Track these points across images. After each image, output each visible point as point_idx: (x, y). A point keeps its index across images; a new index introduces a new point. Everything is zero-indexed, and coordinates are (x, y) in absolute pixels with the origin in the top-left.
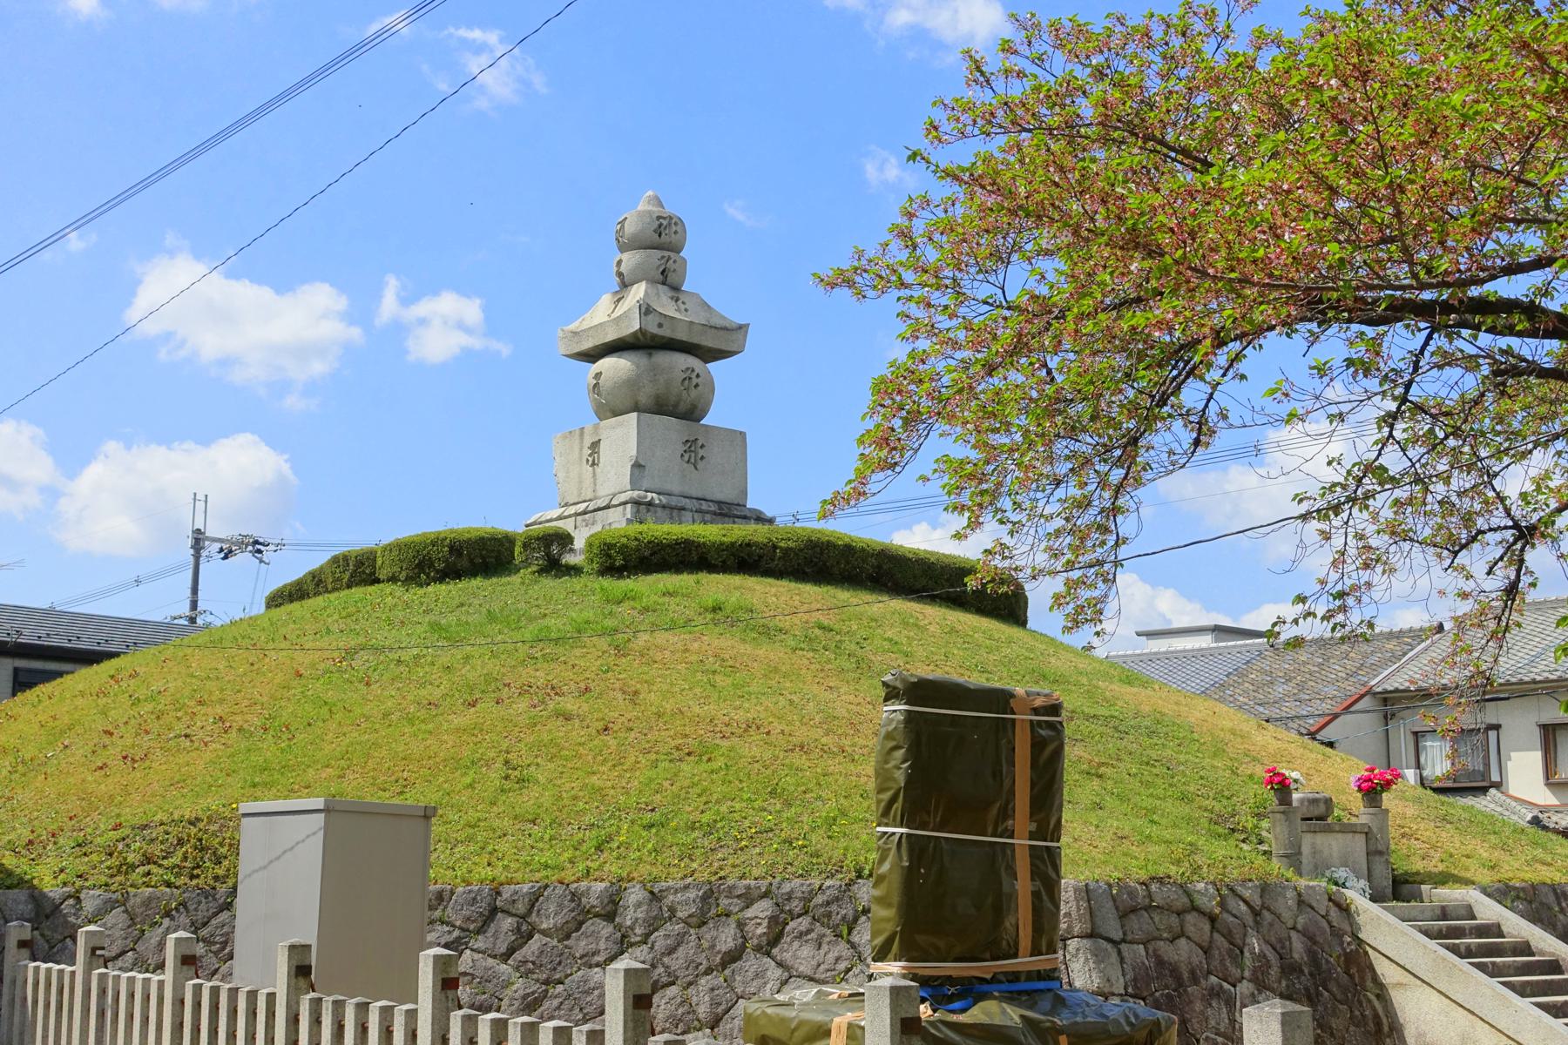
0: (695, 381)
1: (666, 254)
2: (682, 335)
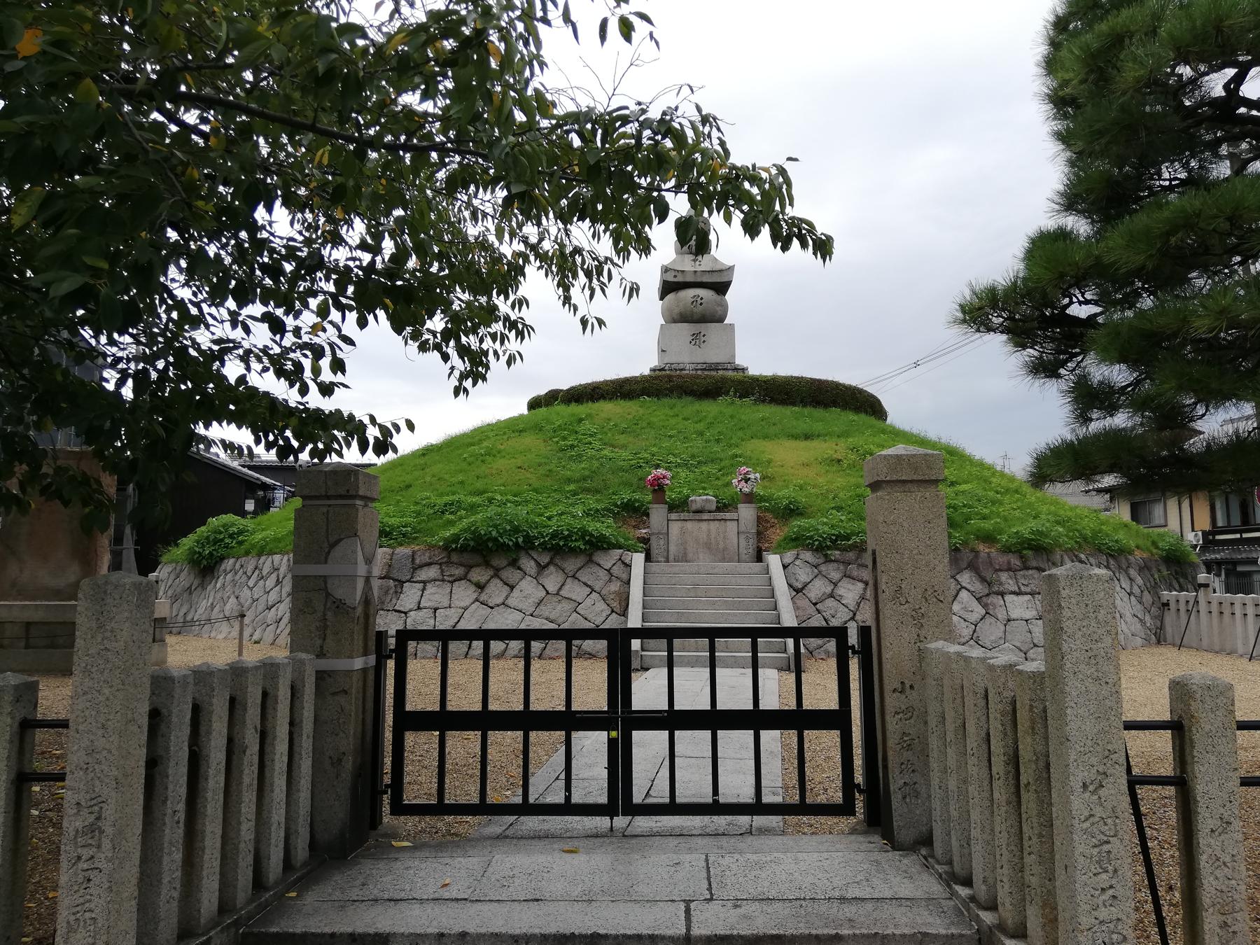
2: (689, 279)
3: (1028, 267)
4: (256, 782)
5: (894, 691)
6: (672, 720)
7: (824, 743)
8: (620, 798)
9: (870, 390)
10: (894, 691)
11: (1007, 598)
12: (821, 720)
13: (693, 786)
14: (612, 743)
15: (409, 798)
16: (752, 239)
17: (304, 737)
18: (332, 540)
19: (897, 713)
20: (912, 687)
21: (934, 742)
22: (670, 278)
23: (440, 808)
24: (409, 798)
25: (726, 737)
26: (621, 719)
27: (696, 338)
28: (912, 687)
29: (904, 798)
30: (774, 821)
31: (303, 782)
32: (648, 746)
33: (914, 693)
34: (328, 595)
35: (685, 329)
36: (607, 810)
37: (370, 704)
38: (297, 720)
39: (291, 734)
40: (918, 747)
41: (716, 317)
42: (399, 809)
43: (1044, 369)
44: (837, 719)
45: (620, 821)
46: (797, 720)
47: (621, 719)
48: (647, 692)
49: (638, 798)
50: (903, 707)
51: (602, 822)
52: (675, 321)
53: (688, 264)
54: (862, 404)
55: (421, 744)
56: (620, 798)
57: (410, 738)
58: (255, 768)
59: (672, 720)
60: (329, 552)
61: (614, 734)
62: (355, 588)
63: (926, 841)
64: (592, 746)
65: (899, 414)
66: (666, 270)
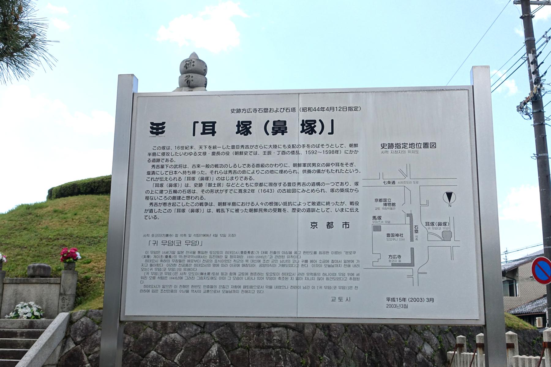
1: (188, 74)
16: (194, 54)
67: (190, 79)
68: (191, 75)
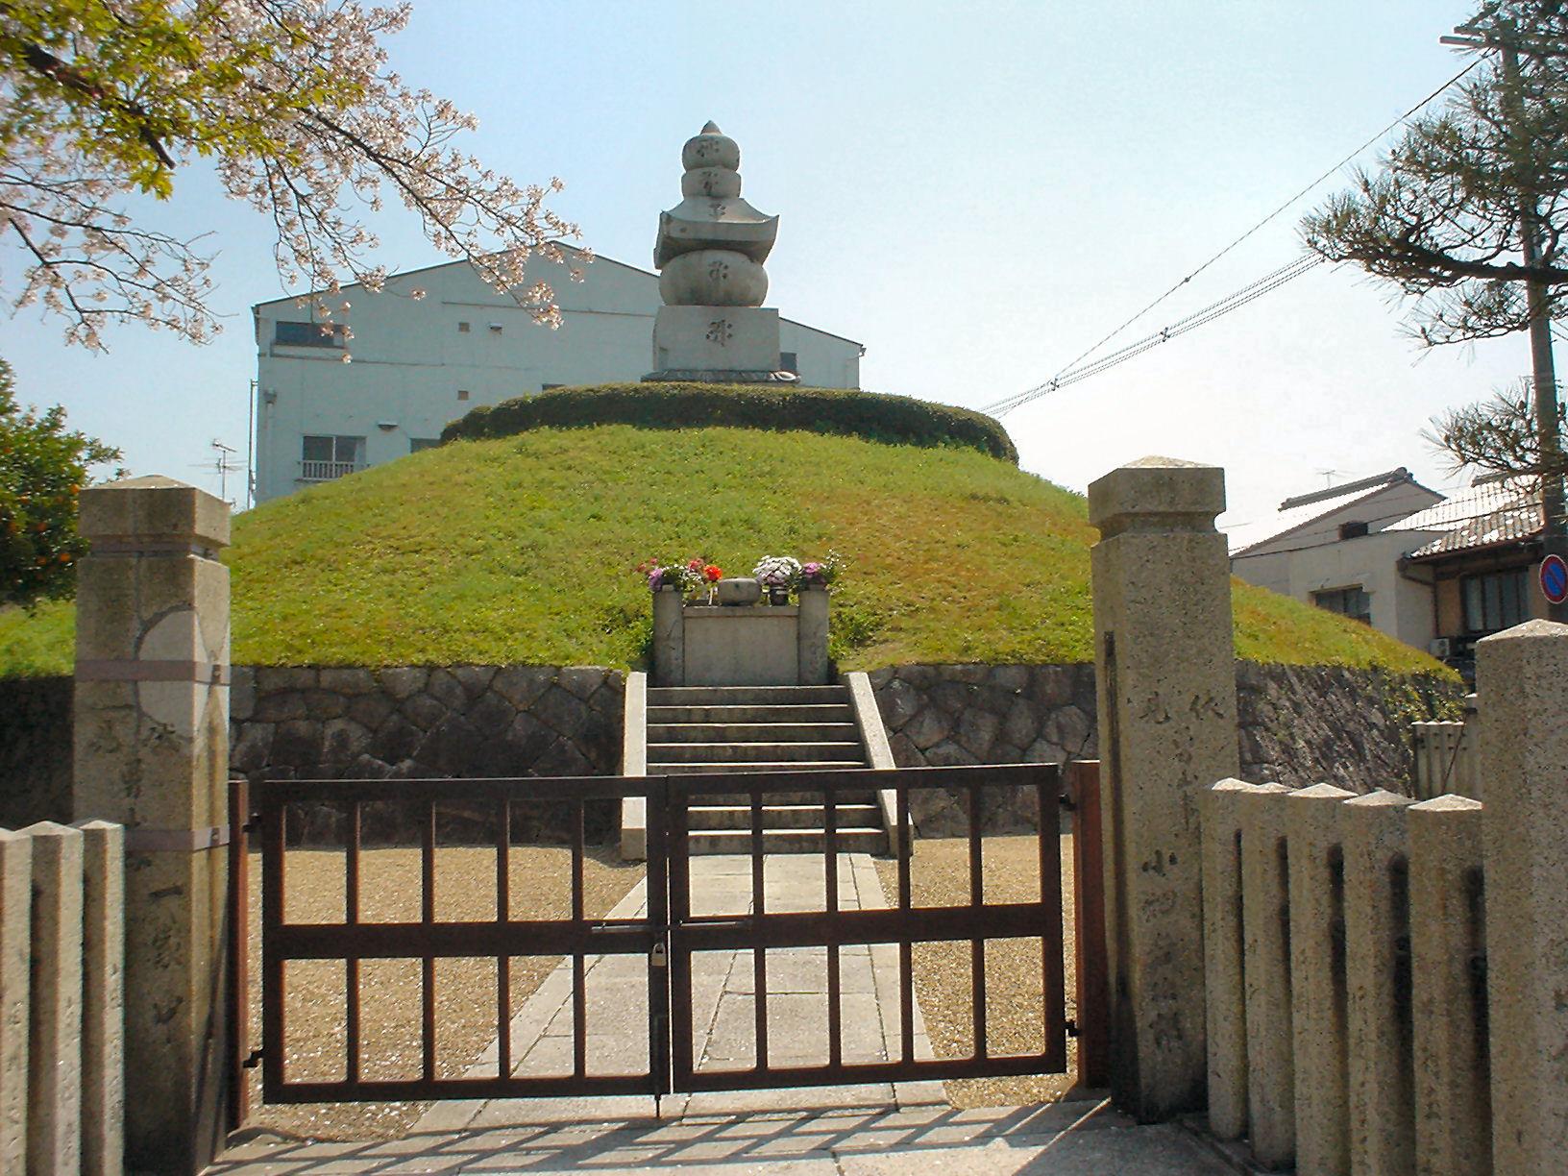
0: (722, 271)
2: (707, 235)
3: (113, 499)
4: (24, 1051)
5: (1145, 868)
6: (761, 932)
7: (1017, 961)
8: (671, 1065)
9: (995, 417)
10: (1145, 868)
11: (843, 1159)
12: (1012, 921)
13: (798, 1043)
14: (656, 976)
15: (296, 1071)
16: (709, 127)
17: (109, 969)
18: (147, 615)
19: (1148, 903)
20: (1173, 860)
21: (1219, 947)
22: (676, 234)
23: (353, 1090)
24: (296, 1071)
25: (851, 955)
26: (671, 937)
27: (718, 331)
28: (1173, 860)
29: (1158, 1043)
30: (934, 1088)
31: (108, 1049)
32: (717, 978)
33: (1176, 869)
34: (142, 715)
35: (697, 317)
36: (652, 1084)
37: (220, 913)
38: (95, 938)
39: (85, 962)
40: (1181, 963)
41: (745, 297)
42: (278, 1091)
43: (1102, 489)
44: (1039, 920)
45: (673, 1103)
46: (978, 922)
47: (671, 937)
48: (717, 886)
49: (700, 1064)
50: (1159, 893)
51: (641, 1105)
52: (680, 302)
53: (703, 214)
54: (981, 436)
55: (313, 981)
56: (671, 1065)
57: (297, 971)
58: (23, 1028)
59: (761, 932)
60: (140, 639)
61: (660, 960)
62: (190, 705)
63: (1195, 1100)
64: (621, 981)
65: (1027, 463)
66: (666, 219)
67: (713, 180)
68: (713, 170)
